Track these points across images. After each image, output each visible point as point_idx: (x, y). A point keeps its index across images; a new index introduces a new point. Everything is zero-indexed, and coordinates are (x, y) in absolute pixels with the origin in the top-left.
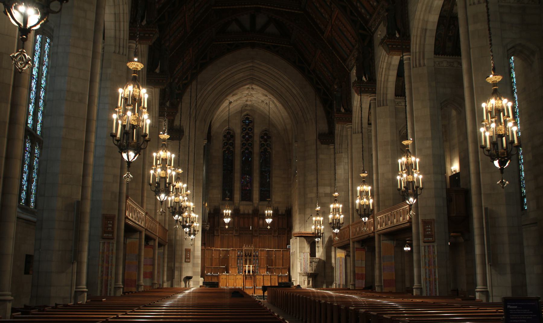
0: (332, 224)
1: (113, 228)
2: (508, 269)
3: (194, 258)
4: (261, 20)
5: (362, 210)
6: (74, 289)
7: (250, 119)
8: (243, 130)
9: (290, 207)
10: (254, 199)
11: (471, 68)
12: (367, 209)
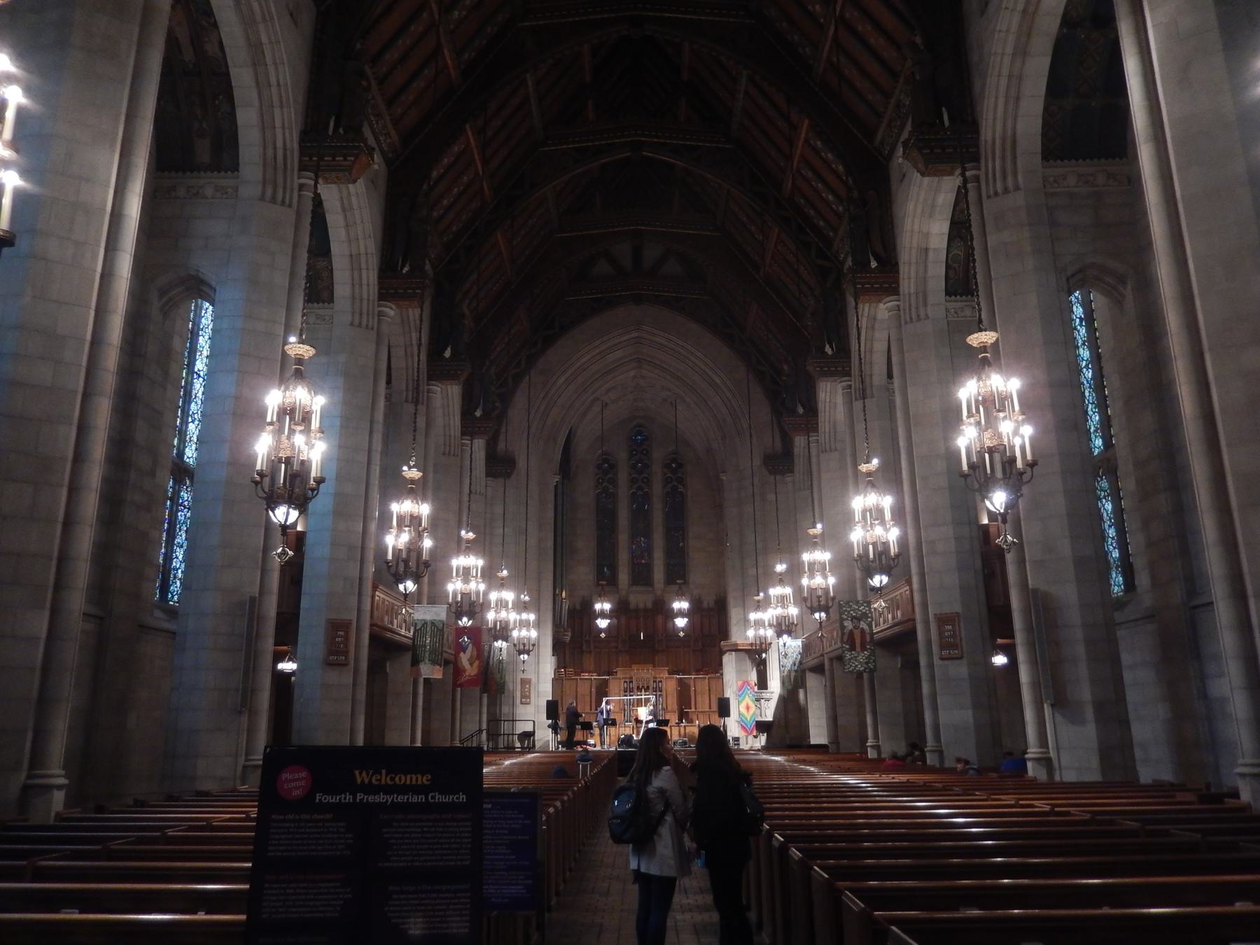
0: (493, 631)
1: (346, 646)
2: (1089, 713)
5: (815, 600)
6: (242, 760)
7: (645, 434)
10: (656, 581)
12: (809, 598)
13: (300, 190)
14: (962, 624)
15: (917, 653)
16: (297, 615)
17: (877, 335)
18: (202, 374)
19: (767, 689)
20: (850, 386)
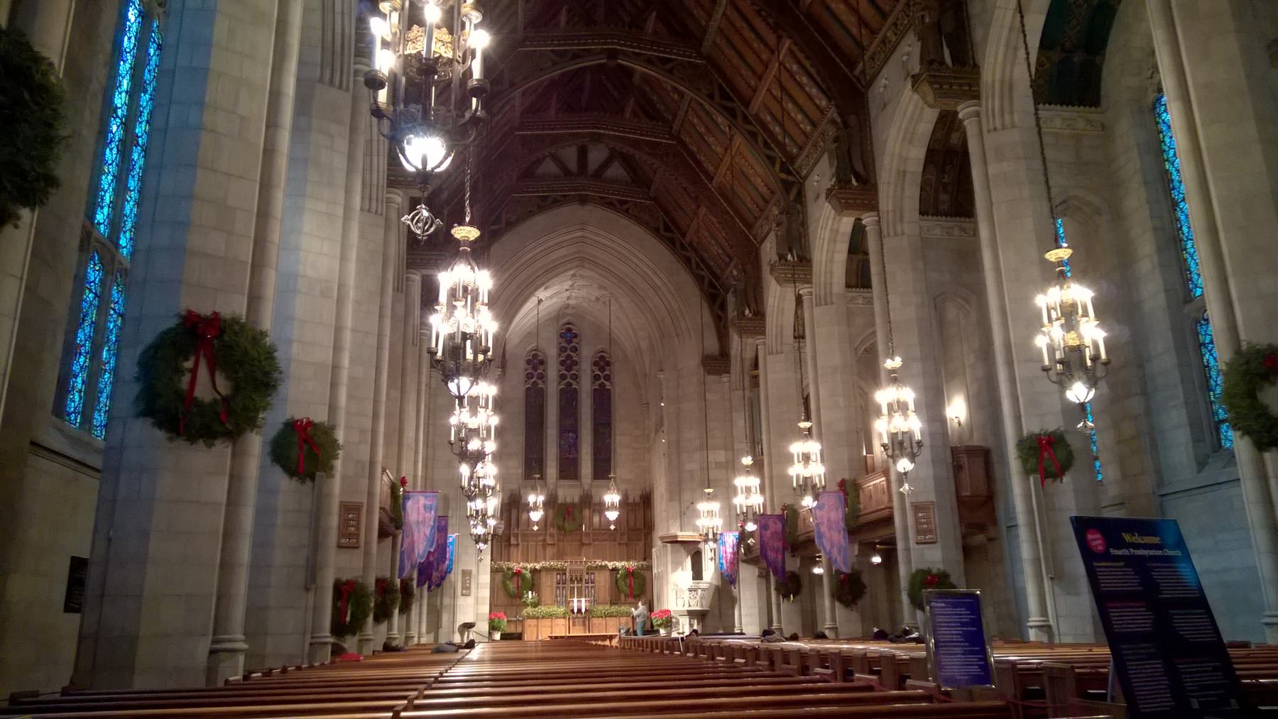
3: (478, 588)
4: (596, 156)
6: (308, 640)
8: (561, 350)
9: (648, 490)
11: (995, 237)
13: (355, 76)
14: (936, 512)
19: (702, 579)
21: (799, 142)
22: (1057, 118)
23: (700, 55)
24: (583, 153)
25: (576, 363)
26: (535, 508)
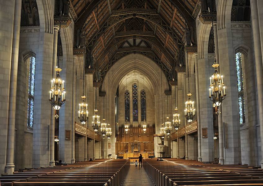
4: (138, 41)
13: (54, 29)
15: (197, 137)
16: (58, 129)
17: (192, 62)
18: (33, 74)
20: (216, 25)
21: (182, 34)
22: (237, 24)
23: (157, 13)
24: (134, 41)
25: (137, 93)
26: (126, 128)
